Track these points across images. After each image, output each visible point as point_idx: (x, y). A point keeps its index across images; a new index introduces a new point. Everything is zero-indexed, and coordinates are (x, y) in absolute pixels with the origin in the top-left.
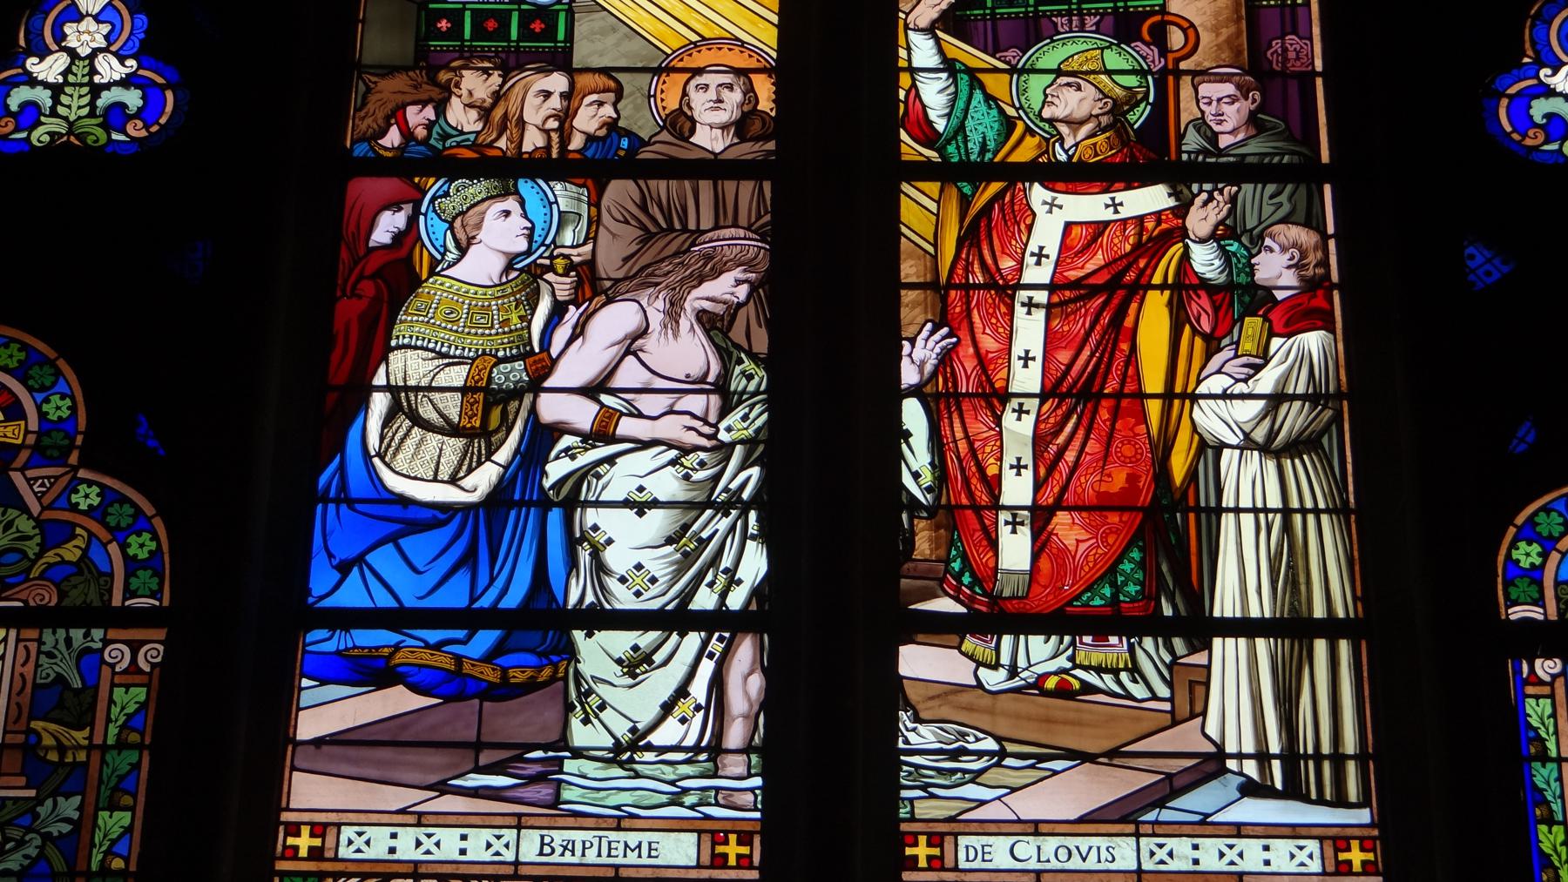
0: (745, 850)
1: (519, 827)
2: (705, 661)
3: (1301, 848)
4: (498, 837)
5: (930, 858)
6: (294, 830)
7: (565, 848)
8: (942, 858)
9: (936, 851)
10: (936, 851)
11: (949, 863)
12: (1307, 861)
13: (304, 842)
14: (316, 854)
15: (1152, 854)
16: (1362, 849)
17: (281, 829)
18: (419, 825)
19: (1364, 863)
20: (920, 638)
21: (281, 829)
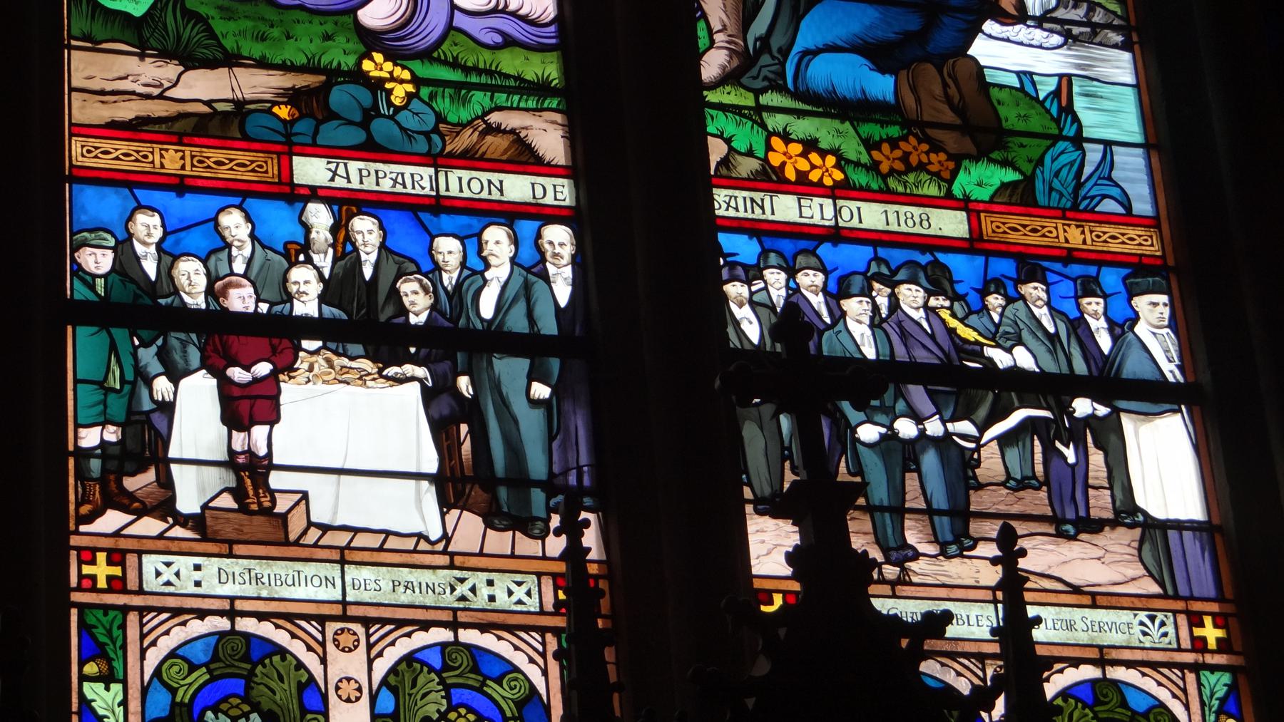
0: (87, 570)
1: (343, 562)
2: (867, 251)
3: (462, 580)
4: (168, 564)
5: (110, 579)
6: (88, 555)
7: (407, 587)
8: (123, 579)
9: (117, 571)
10: (117, 571)
11: (132, 584)
12: (525, 599)
13: (102, 570)
14: (117, 585)
15: (158, 574)
16: (1216, 626)
17: (73, 554)
18: (452, 566)
19: (1218, 640)
20: (1155, 160)
21: (73, 554)
